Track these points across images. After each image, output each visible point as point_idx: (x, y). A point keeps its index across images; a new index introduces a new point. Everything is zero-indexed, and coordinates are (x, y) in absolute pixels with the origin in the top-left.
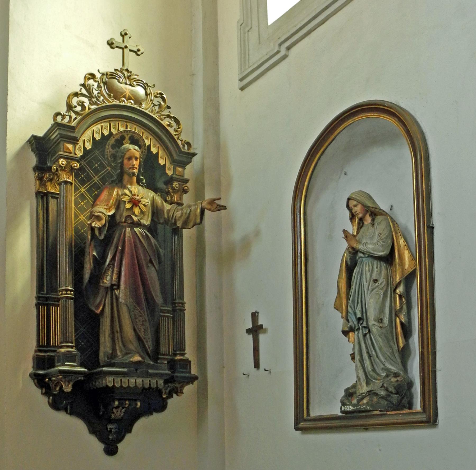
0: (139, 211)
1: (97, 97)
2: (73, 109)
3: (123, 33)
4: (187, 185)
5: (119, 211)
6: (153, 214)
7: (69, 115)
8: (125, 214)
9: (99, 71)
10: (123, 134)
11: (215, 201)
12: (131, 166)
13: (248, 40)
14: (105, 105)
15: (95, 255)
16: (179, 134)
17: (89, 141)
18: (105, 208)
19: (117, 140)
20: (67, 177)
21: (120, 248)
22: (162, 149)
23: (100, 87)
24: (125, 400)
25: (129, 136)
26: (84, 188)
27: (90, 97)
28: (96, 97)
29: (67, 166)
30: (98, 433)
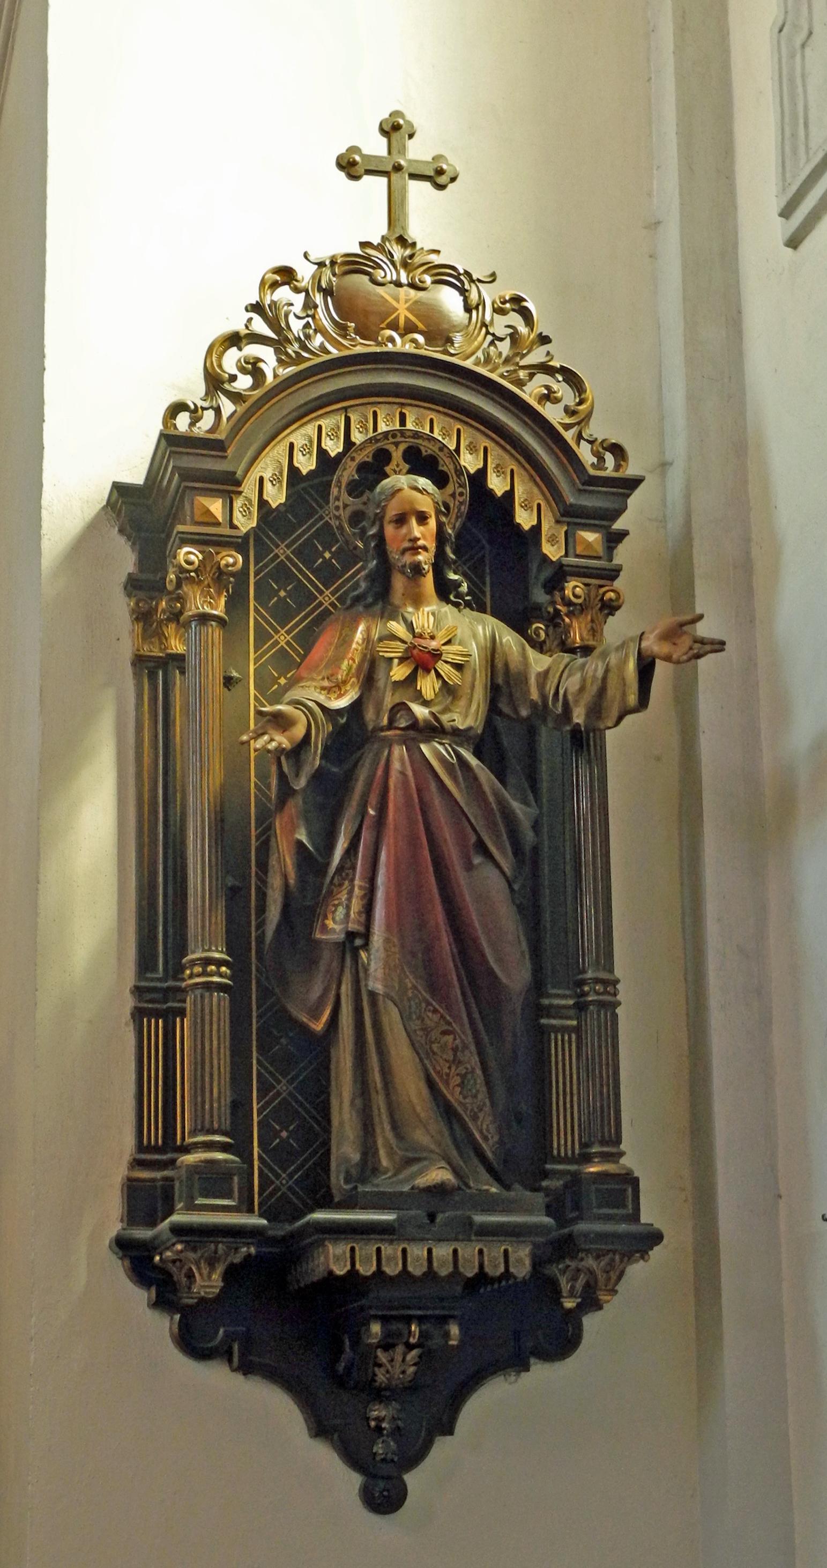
0: (438, 685)
1: (303, 338)
2: (227, 386)
3: (387, 128)
4: (617, 584)
5: (374, 693)
6: (494, 691)
7: (211, 407)
8: (389, 701)
9: (306, 256)
10: (379, 444)
11: (685, 628)
12: (407, 544)
13: (803, 76)
14: (326, 357)
15: (305, 841)
16: (583, 420)
17: (275, 480)
18: (323, 688)
19: (362, 468)
20: (204, 602)
21: (372, 812)
22: (527, 478)
23: (311, 305)
24: (408, 1320)
25: (402, 447)
26: (288, 632)
27: (279, 343)
28: (298, 339)
29: (205, 567)
30: (336, 1436)
